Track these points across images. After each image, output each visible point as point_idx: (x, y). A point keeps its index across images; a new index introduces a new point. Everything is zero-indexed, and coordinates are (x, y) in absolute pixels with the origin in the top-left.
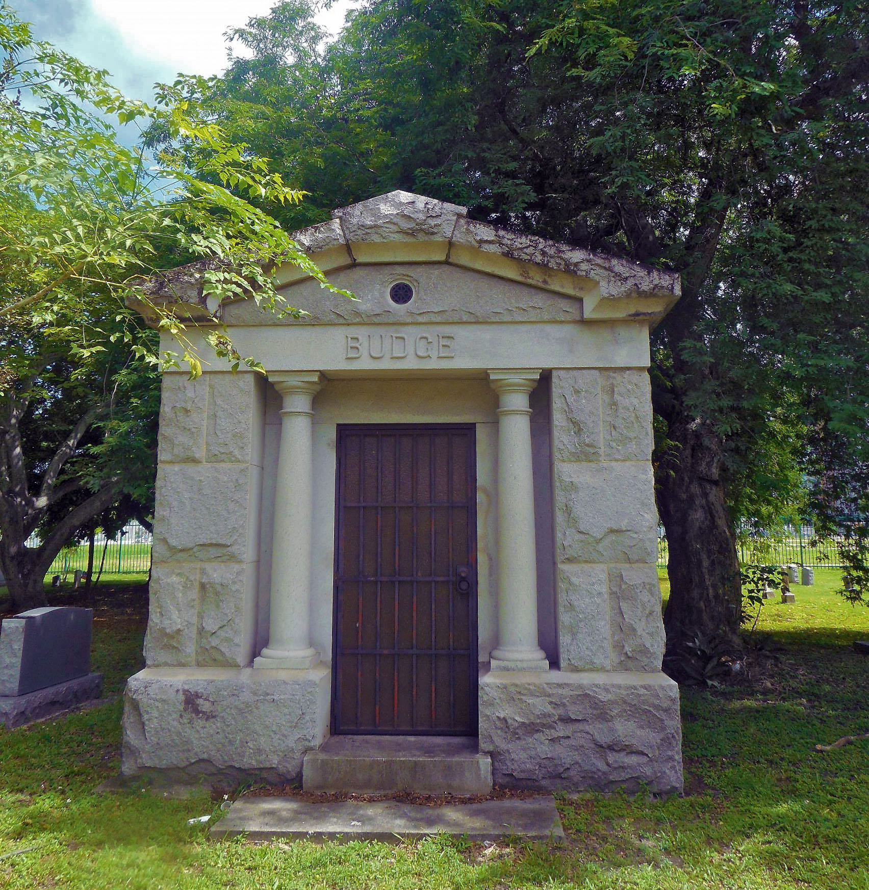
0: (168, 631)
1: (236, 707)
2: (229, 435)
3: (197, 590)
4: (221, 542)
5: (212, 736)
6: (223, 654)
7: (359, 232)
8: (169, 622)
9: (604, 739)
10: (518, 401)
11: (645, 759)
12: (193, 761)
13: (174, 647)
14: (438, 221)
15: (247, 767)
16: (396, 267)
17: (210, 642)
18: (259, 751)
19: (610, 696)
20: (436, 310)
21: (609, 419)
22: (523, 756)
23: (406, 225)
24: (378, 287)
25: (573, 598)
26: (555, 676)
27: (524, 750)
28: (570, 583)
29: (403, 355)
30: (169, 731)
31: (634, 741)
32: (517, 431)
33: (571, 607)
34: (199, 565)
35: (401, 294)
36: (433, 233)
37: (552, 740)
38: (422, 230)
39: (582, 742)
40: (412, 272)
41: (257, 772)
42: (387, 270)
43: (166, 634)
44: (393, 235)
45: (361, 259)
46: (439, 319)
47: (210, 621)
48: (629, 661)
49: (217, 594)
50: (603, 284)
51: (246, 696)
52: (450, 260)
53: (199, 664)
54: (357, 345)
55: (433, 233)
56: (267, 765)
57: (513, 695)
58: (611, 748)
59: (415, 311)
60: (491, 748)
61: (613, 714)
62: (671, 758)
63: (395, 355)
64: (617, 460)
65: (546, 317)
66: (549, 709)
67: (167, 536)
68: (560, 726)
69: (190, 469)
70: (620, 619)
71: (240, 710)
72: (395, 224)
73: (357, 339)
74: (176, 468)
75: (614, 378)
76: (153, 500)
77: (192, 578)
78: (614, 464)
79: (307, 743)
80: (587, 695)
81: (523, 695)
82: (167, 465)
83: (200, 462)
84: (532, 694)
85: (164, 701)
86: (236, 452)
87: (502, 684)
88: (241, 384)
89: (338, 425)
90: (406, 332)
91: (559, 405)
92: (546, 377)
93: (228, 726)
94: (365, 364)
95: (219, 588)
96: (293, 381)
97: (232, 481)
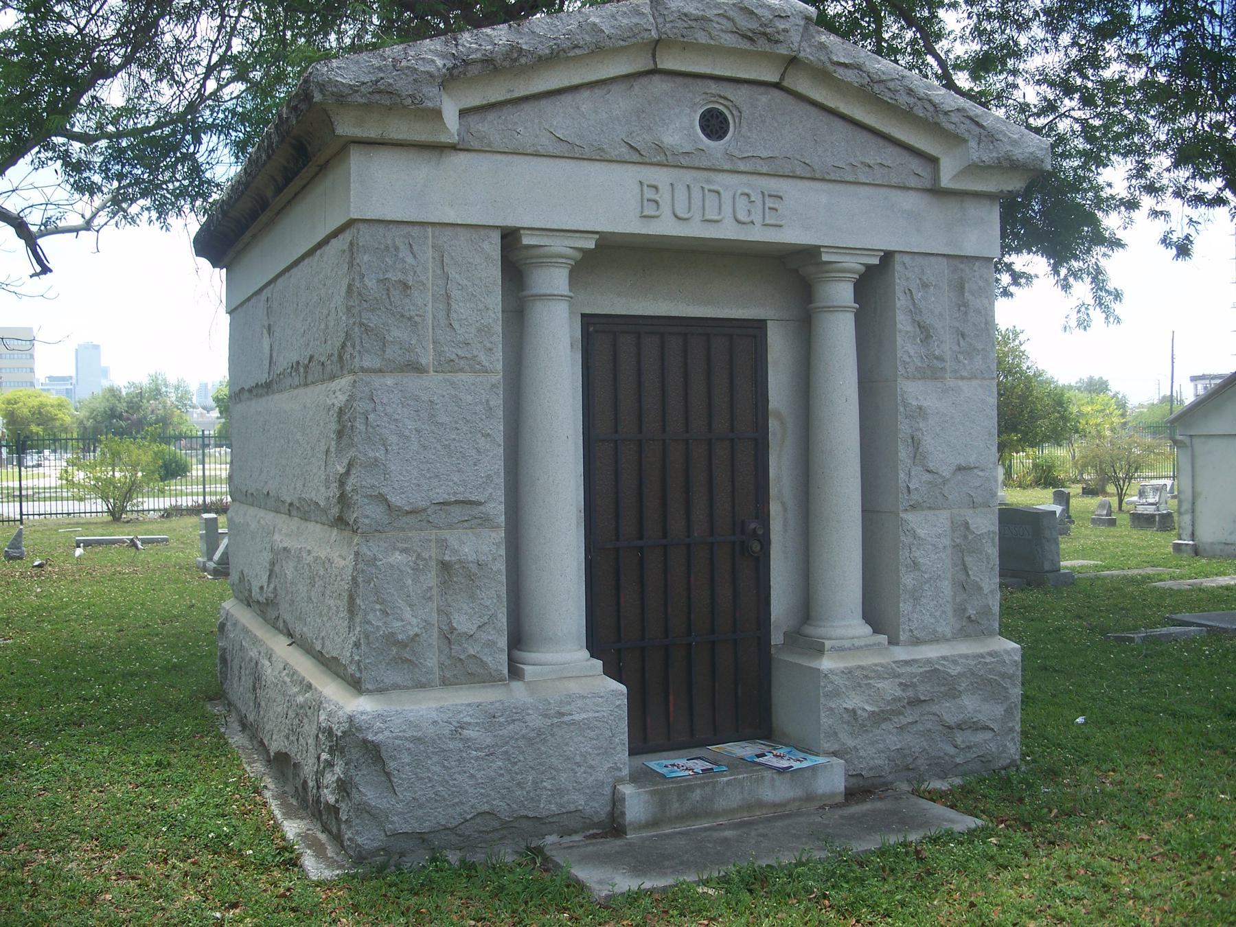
0: (400, 637)
1: (524, 736)
2: (473, 330)
3: (434, 573)
4: (473, 498)
5: (493, 780)
6: (483, 664)
7: (680, 24)
8: (400, 624)
9: (951, 720)
10: (843, 293)
11: (989, 735)
12: (469, 817)
13: (407, 660)
14: (787, 26)
15: (545, 813)
17: (464, 650)
18: (560, 791)
19: (959, 669)
20: (765, 154)
21: (957, 324)
22: (871, 751)
23: (745, 23)
24: (688, 111)
25: (918, 554)
26: (901, 653)
27: (872, 743)
28: (915, 536)
29: (686, 216)
31: (980, 717)
32: (840, 335)
33: (915, 565)
34: (433, 534)
35: (714, 125)
36: (777, 42)
38: (765, 34)
39: (929, 725)
40: (739, 95)
41: (555, 819)
42: (700, 86)
43: (397, 643)
44: (722, 35)
46: (765, 169)
47: (463, 618)
48: (970, 627)
49: (471, 577)
50: (973, 144)
51: (535, 721)
52: (785, 83)
53: (445, 683)
54: (656, 197)
55: (777, 42)
56: (572, 808)
57: (858, 679)
58: (959, 727)
59: (736, 153)
60: (836, 747)
61: (961, 689)
62: (1012, 730)
63: (708, 217)
64: (962, 378)
65: (894, 181)
66: (899, 693)
67: (384, 490)
68: (908, 711)
69: (412, 382)
70: (963, 578)
71: (530, 739)
72: (728, 18)
73: (656, 188)
74: (389, 381)
75: (962, 270)
77: (426, 555)
78: (960, 383)
79: (617, 773)
80: (936, 670)
81: (871, 678)
82: (373, 375)
83: (427, 372)
84: (880, 677)
85: (419, 739)
86: (482, 357)
87: (846, 668)
88: (486, 245)
89: (583, 315)
90: (723, 181)
91: (903, 302)
92: (887, 257)
93: (516, 763)
94: (665, 227)
96: (559, 245)
97: (481, 403)
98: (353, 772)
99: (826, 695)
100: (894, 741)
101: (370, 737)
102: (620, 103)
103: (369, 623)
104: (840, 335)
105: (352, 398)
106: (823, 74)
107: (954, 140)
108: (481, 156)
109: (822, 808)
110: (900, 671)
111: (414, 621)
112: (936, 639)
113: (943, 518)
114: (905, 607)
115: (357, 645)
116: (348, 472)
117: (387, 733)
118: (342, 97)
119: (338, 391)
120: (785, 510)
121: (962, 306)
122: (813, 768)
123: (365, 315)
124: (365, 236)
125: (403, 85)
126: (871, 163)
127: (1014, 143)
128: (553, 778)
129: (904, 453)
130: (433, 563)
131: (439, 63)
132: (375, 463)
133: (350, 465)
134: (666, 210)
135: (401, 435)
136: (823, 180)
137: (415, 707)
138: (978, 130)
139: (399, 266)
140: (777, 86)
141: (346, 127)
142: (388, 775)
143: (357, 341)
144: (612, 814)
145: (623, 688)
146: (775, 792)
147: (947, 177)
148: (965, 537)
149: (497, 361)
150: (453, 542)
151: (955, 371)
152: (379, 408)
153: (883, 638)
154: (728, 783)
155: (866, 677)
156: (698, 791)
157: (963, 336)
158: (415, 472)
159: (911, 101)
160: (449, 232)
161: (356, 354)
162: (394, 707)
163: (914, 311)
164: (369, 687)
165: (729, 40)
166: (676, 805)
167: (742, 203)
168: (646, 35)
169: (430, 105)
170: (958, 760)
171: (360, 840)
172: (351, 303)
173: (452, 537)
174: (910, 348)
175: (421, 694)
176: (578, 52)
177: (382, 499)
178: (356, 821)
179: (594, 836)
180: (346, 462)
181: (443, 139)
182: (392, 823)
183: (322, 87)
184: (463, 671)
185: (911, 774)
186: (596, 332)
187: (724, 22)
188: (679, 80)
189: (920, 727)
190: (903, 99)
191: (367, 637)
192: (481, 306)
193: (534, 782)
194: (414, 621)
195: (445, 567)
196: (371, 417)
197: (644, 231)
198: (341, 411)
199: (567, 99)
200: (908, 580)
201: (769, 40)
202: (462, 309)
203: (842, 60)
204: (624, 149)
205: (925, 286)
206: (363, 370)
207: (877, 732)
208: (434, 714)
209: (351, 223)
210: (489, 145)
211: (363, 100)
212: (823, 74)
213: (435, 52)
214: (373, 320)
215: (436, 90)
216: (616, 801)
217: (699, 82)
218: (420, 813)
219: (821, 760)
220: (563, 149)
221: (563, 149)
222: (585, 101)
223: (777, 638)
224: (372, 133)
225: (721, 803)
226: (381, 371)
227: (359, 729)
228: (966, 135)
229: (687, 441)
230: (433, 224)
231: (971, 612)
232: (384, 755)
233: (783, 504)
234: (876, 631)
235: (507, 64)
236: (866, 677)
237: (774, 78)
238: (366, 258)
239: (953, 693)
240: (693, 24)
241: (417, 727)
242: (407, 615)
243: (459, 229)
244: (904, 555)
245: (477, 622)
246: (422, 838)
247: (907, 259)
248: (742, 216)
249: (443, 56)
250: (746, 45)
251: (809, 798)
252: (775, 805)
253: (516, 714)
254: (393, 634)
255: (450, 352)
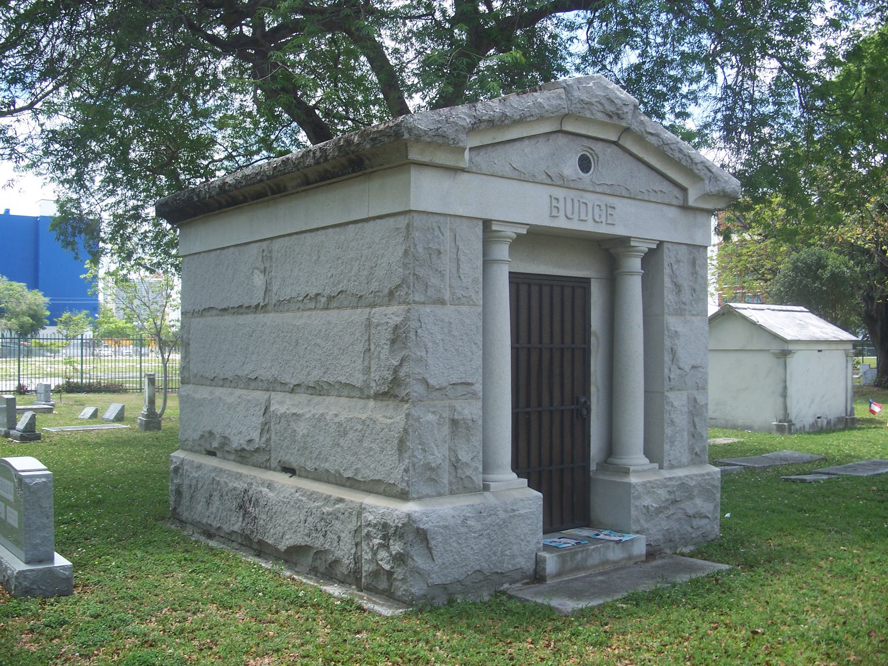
0: (433, 465)
1: (497, 524)
2: (470, 280)
7: (579, 106)
9: (691, 512)
10: (635, 264)
11: (707, 521)
16: (584, 139)
17: (464, 473)
18: (513, 557)
23: (610, 108)
26: (667, 474)
27: (655, 526)
30: (451, 551)
34: (447, 402)
35: (585, 164)
37: (668, 517)
38: (617, 114)
39: (680, 515)
40: (598, 147)
45: (567, 127)
46: (608, 192)
49: (468, 429)
50: (707, 182)
51: (502, 515)
52: (620, 142)
53: (452, 493)
54: (558, 205)
55: (622, 119)
57: (649, 488)
60: (639, 528)
65: (666, 201)
69: (439, 310)
70: (692, 429)
71: (499, 526)
72: (601, 104)
73: (558, 200)
74: (428, 309)
76: (707, 382)
78: (693, 318)
80: (683, 483)
84: (658, 487)
86: (474, 297)
90: (589, 198)
92: (661, 243)
94: (562, 223)
95: (470, 423)
98: (409, 549)
99: (634, 498)
100: (665, 525)
101: (421, 526)
102: (543, 149)
103: (416, 457)
104: (633, 289)
105: (406, 319)
106: (640, 139)
107: (696, 178)
108: (475, 175)
109: (636, 563)
110: (668, 483)
111: (439, 455)
112: (681, 466)
113: (685, 393)
114: (667, 447)
115: (406, 471)
116: (401, 365)
117: (430, 523)
118: (418, 137)
119: (392, 314)
120: (598, 390)
121: (694, 273)
122: (632, 540)
123: (417, 269)
124: (417, 221)
125: (450, 132)
126: (657, 190)
127: (726, 182)
128: (510, 549)
129: (667, 358)
130: (447, 420)
131: (468, 120)
132: (420, 360)
133: (402, 361)
134: (562, 212)
135: (434, 342)
136: (634, 199)
137: (438, 508)
138: (709, 174)
139: (437, 240)
140: (615, 143)
141: (414, 155)
142: (429, 549)
143: (412, 284)
144: (535, 571)
145: (540, 494)
146: (615, 554)
147: (692, 199)
148: (695, 407)
149: (479, 299)
150: (459, 408)
151: (690, 311)
152: (423, 325)
153: (656, 465)
154: (594, 550)
155: (652, 487)
156: (580, 555)
157: (694, 290)
158: (441, 365)
159: (681, 156)
160: (458, 220)
161: (410, 292)
162: (430, 508)
163: (673, 275)
164: (414, 496)
165: (600, 117)
166: (569, 563)
167: (597, 209)
168: (563, 111)
169: (462, 145)
170: (693, 536)
171: (413, 590)
172: (407, 261)
173: (458, 404)
174: (670, 297)
175: (441, 500)
176: (532, 118)
177: (425, 381)
178: (410, 579)
179: (527, 583)
180: (399, 358)
181: (461, 165)
182: (432, 578)
183: (410, 130)
184: (463, 486)
185: (672, 544)
186: (516, 279)
187: (599, 105)
188: (570, 137)
189: (676, 517)
190: (677, 155)
191: (414, 465)
192: (474, 266)
193: (502, 552)
194: (439, 455)
195: (454, 422)
196: (419, 331)
197: (551, 225)
198: (396, 327)
199: (518, 144)
200: (668, 431)
201: (619, 117)
202: (465, 267)
203: (651, 131)
204: (545, 176)
205: (678, 261)
206: (415, 302)
207: (658, 519)
208: (452, 512)
209: (410, 211)
210: (481, 169)
211: (429, 140)
212: (640, 139)
213: (465, 113)
214: (421, 272)
215: (464, 136)
216: (539, 562)
217: (579, 138)
218: (446, 572)
219: (633, 536)
220: (515, 175)
221: (515, 175)
222: (526, 146)
223: (593, 467)
224: (426, 159)
225: (590, 562)
226: (424, 303)
227: (414, 522)
228: (704, 177)
229: (551, 349)
230: (450, 215)
231: (697, 450)
232: (429, 537)
233: (597, 387)
234: (651, 461)
235: (499, 123)
236: (652, 487)
237: (614, 139)
238: (417, 234)
239: (691, 497)
240: (585, 106)
241: (445, 519)
242: (436, 452)
243: (463, 219)
244: (666, 416)
245: (471, 455)
246: (444, 587)
247: (670, 246)
248: (597, 219)
249: (469, 117)
250: (607, 120)
251: (630, 558)
252: (614, 562)
253: (493, 511)
254: (429, 463)
255: (459, 293)
